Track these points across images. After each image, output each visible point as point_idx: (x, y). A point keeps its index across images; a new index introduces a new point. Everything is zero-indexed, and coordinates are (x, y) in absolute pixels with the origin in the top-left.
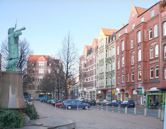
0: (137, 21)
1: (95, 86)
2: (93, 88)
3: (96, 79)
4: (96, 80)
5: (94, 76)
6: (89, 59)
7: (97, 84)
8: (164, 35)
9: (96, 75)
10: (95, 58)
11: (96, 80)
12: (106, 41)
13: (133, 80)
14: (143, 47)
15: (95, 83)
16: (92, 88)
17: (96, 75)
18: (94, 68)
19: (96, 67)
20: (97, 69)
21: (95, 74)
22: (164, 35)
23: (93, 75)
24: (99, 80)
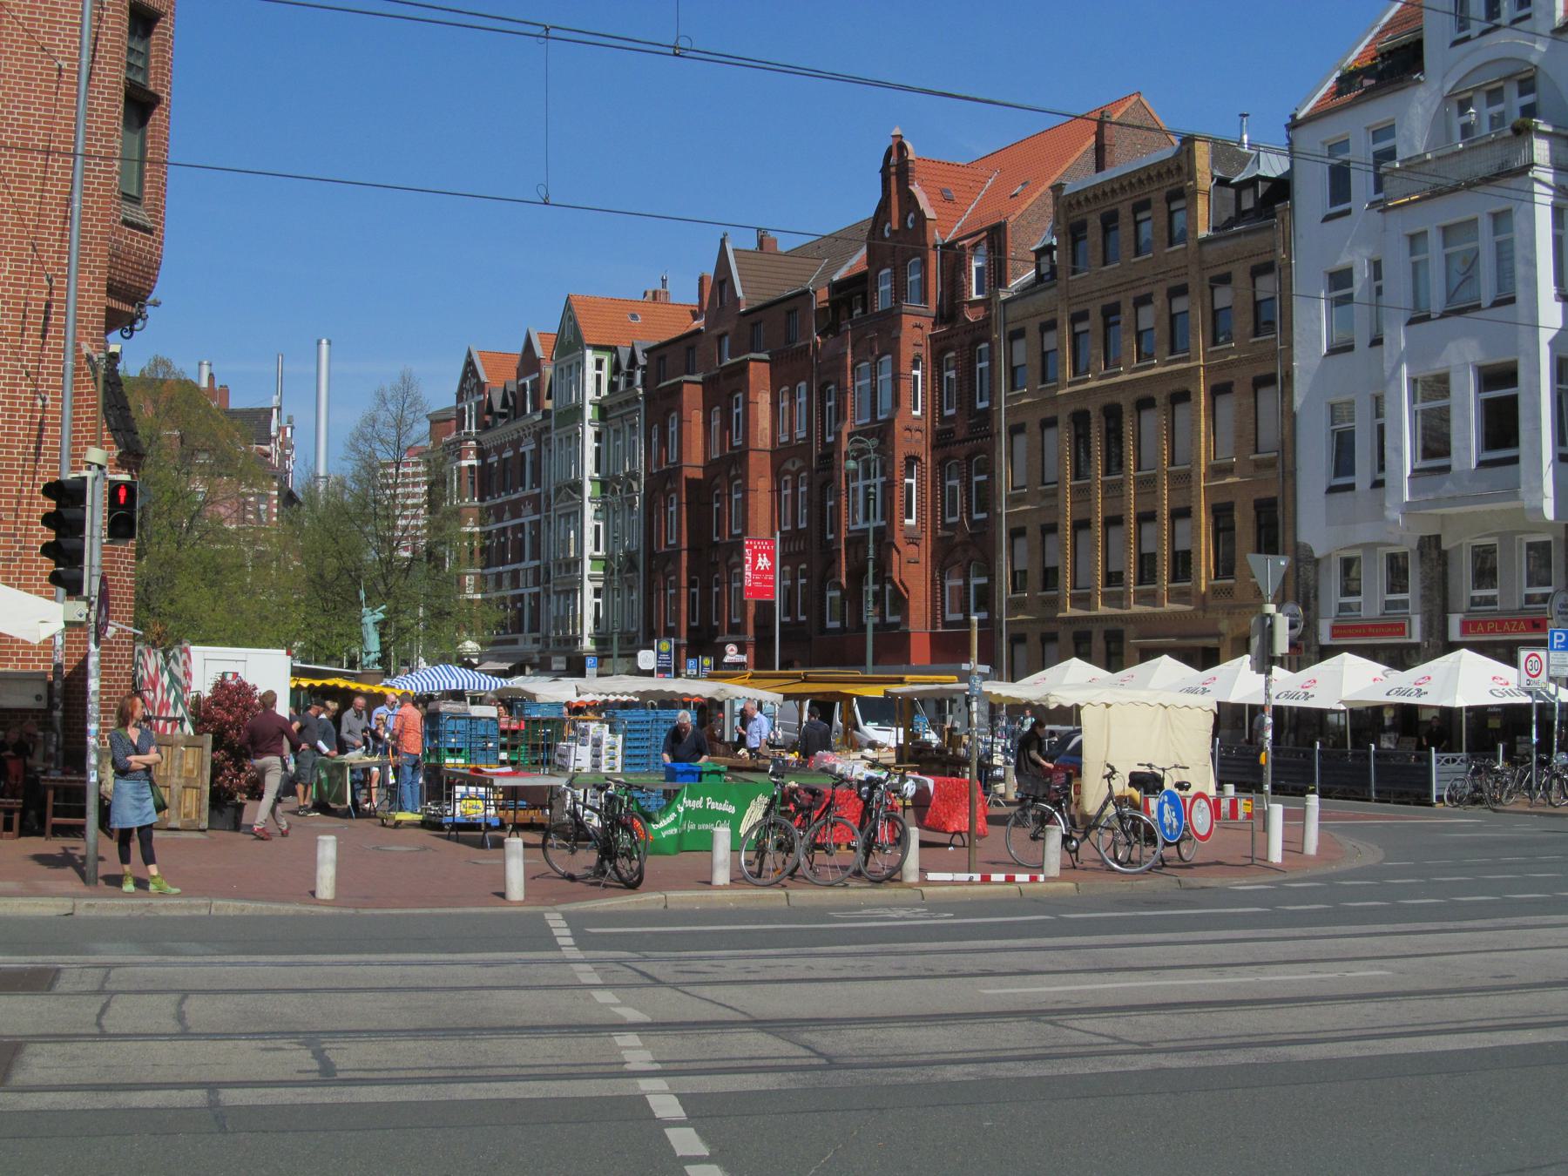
0: (1261, 325)
1: (535, 627)
2: (521, 642)
3: (537, 583)
4: (536, 589)
5: (528, 563)
6: (499, 450)
7: (543, 617)
8: (687, 1168)
9: (537, 563)
10: (537, 453)
11: (536, 589)
12: (598, 377)
13: (910, 486)
14: (1297, 351)
15: (536, 611)
16: (515, 642)
17: (537, 563)
18: (527, 518)
19: (537, 510)
20: (543, 526)
21: (536, 554)
22: (687, 1168)
23: (521, 560)
24: (553, 598)
